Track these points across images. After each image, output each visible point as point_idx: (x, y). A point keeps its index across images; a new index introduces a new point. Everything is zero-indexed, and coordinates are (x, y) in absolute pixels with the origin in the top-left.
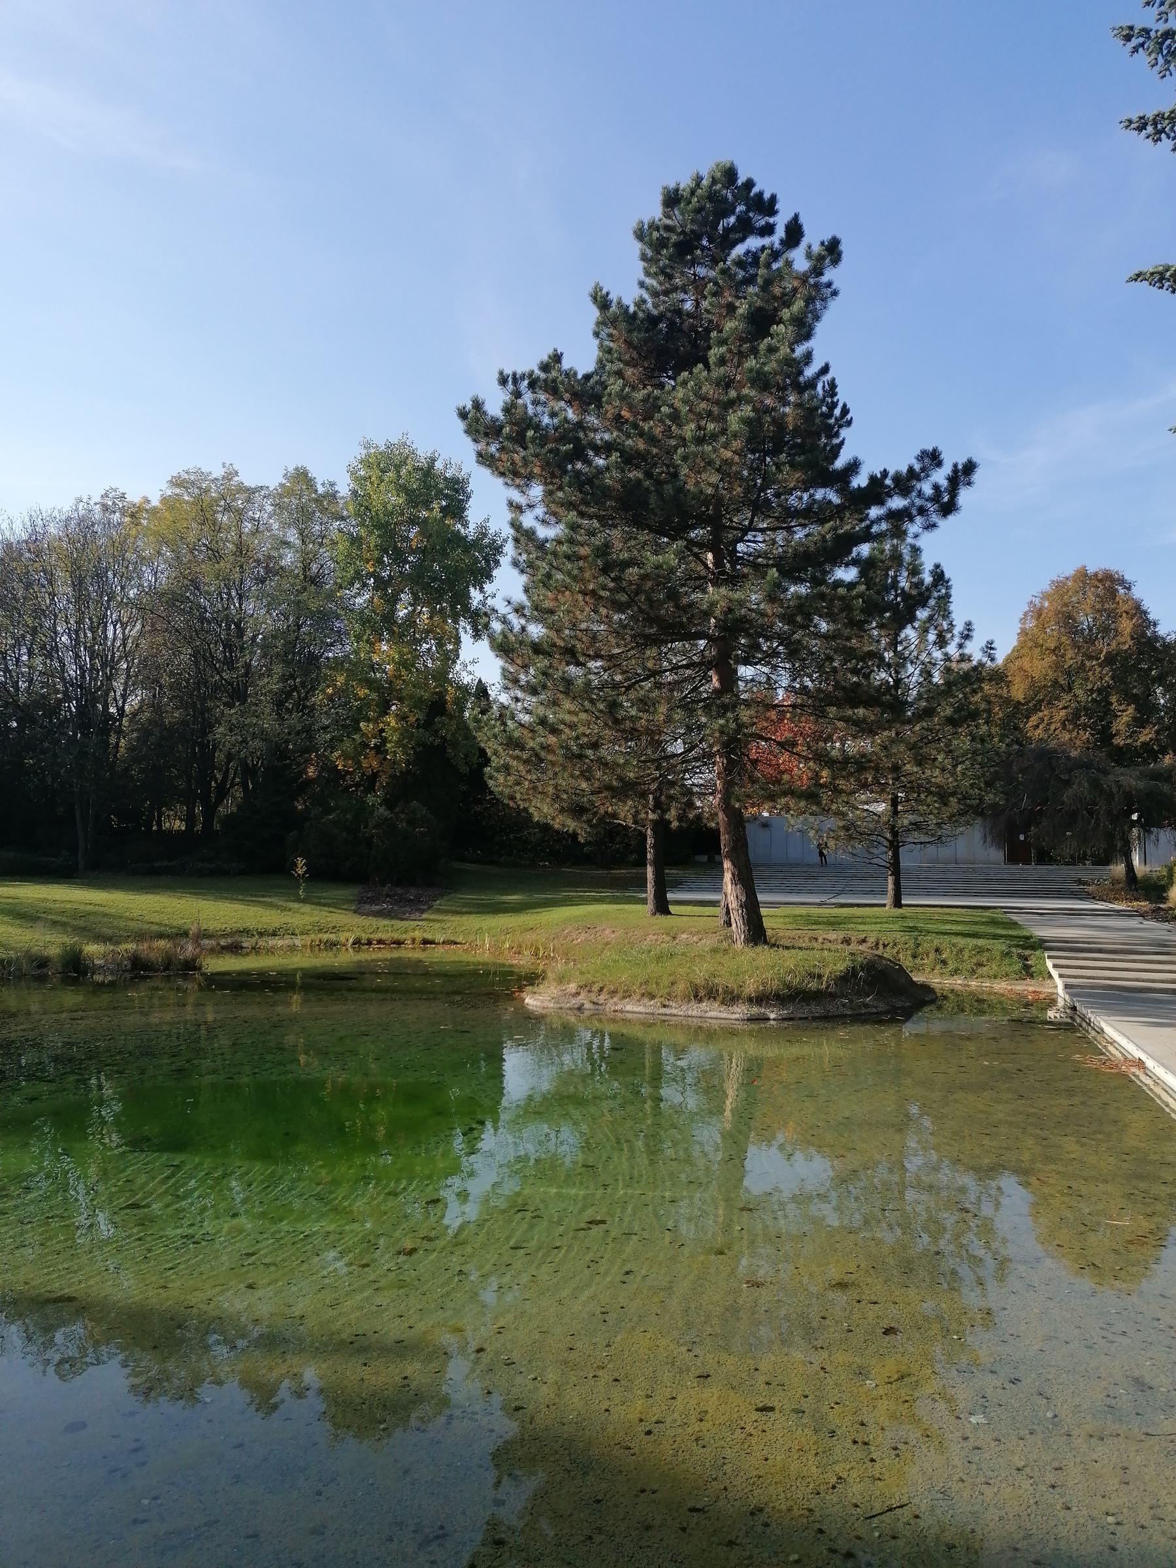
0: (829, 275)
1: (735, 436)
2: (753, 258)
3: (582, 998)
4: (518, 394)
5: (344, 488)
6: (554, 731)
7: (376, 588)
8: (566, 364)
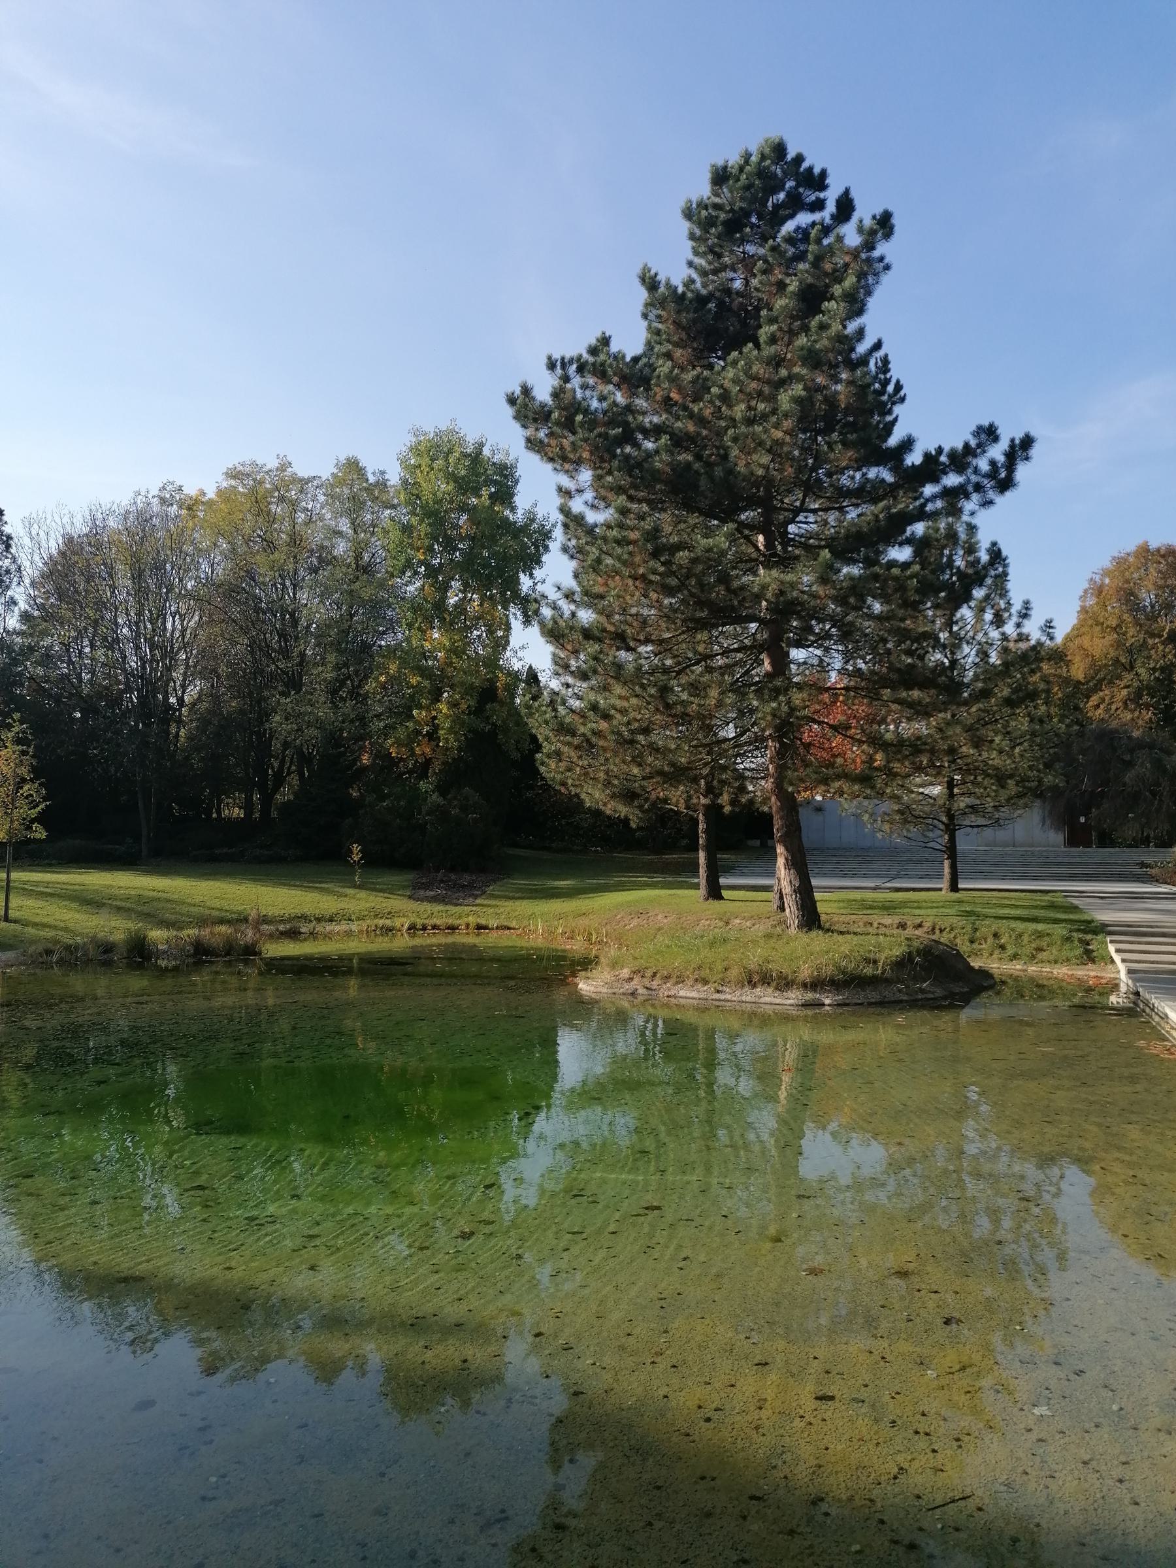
2: (803, 234)
3: (636, 984)
4: (566, 379)
5: (394, 477)
6: (606, 717)
8: (614, 347)
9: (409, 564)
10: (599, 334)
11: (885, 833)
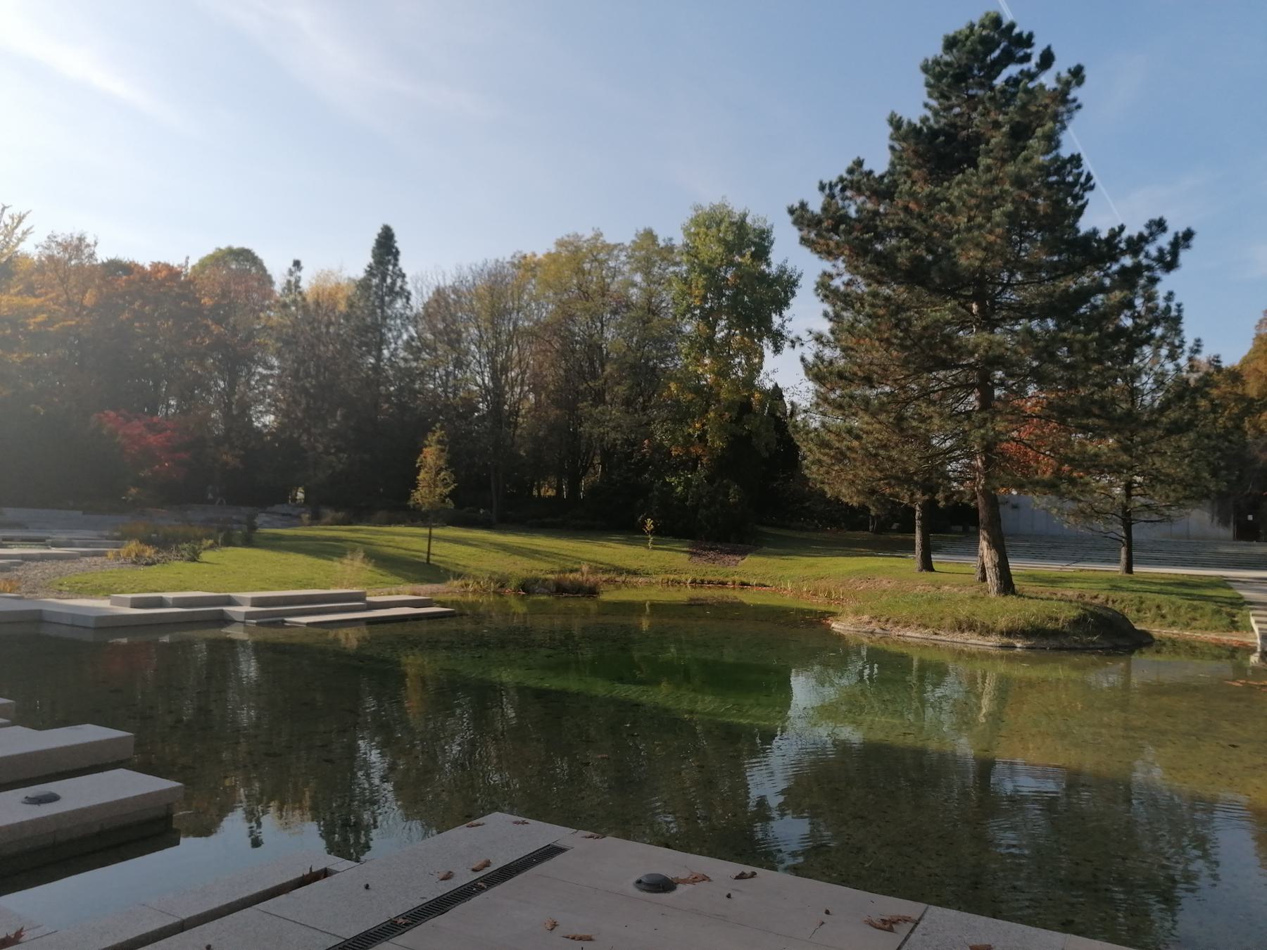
0: (1074, 93)
1: (998, 225)
2: (1013, 82)
3: (874, 625)
4: (832, 196)
5: (679, 240)
6: (858, 438)
7: (701, 317)
8: (866, 167)
9: (689, 309)
10: (855, 158)
11: (1070, 525)
